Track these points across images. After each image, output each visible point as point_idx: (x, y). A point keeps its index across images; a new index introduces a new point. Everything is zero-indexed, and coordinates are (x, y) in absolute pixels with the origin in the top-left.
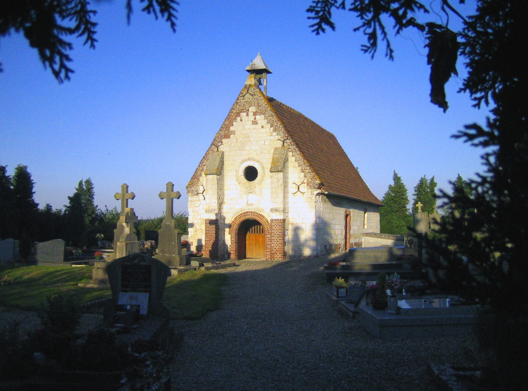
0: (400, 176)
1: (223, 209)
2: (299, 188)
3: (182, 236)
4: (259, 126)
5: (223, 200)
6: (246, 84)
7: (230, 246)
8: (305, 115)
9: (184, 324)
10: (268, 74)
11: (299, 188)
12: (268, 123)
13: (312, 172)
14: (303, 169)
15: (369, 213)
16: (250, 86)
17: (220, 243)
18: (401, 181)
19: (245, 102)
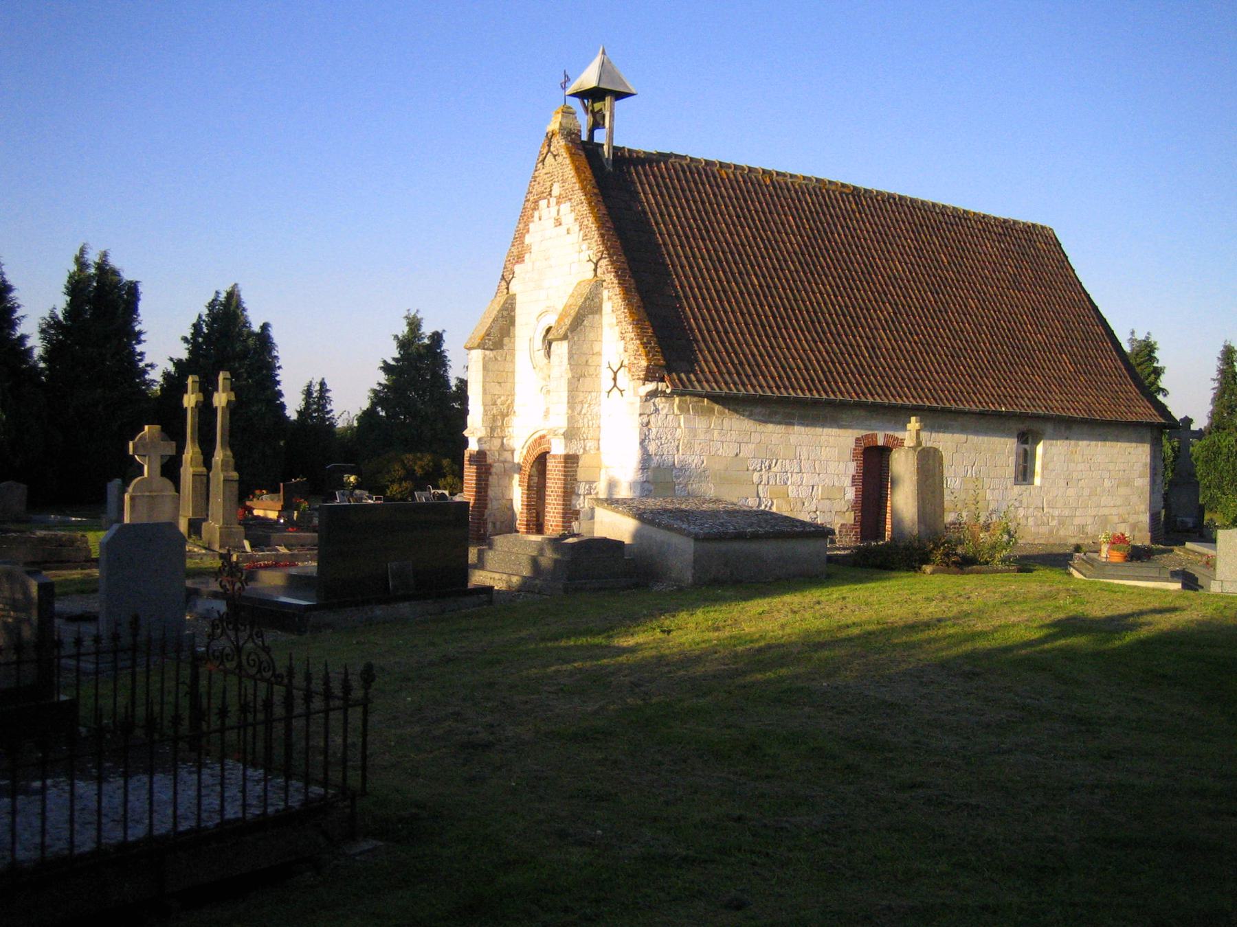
0: (395, 344)
1: (510, 429)
2: (615, 379)
3: (110, 481)
4: (563, 229)
5: (508, 407)
6: (547, 131)
7: (521, 513)
8: (936, 201)
9: (805, 700)
10: (617, 103)
11: (615, 379)
12: (576, 220)
13: (636, 339)
14: (623, 332)
15: (1048, 442)
16: (553, 135)
17: (493, 506)
18: (188, 349)
19: (546, 174)
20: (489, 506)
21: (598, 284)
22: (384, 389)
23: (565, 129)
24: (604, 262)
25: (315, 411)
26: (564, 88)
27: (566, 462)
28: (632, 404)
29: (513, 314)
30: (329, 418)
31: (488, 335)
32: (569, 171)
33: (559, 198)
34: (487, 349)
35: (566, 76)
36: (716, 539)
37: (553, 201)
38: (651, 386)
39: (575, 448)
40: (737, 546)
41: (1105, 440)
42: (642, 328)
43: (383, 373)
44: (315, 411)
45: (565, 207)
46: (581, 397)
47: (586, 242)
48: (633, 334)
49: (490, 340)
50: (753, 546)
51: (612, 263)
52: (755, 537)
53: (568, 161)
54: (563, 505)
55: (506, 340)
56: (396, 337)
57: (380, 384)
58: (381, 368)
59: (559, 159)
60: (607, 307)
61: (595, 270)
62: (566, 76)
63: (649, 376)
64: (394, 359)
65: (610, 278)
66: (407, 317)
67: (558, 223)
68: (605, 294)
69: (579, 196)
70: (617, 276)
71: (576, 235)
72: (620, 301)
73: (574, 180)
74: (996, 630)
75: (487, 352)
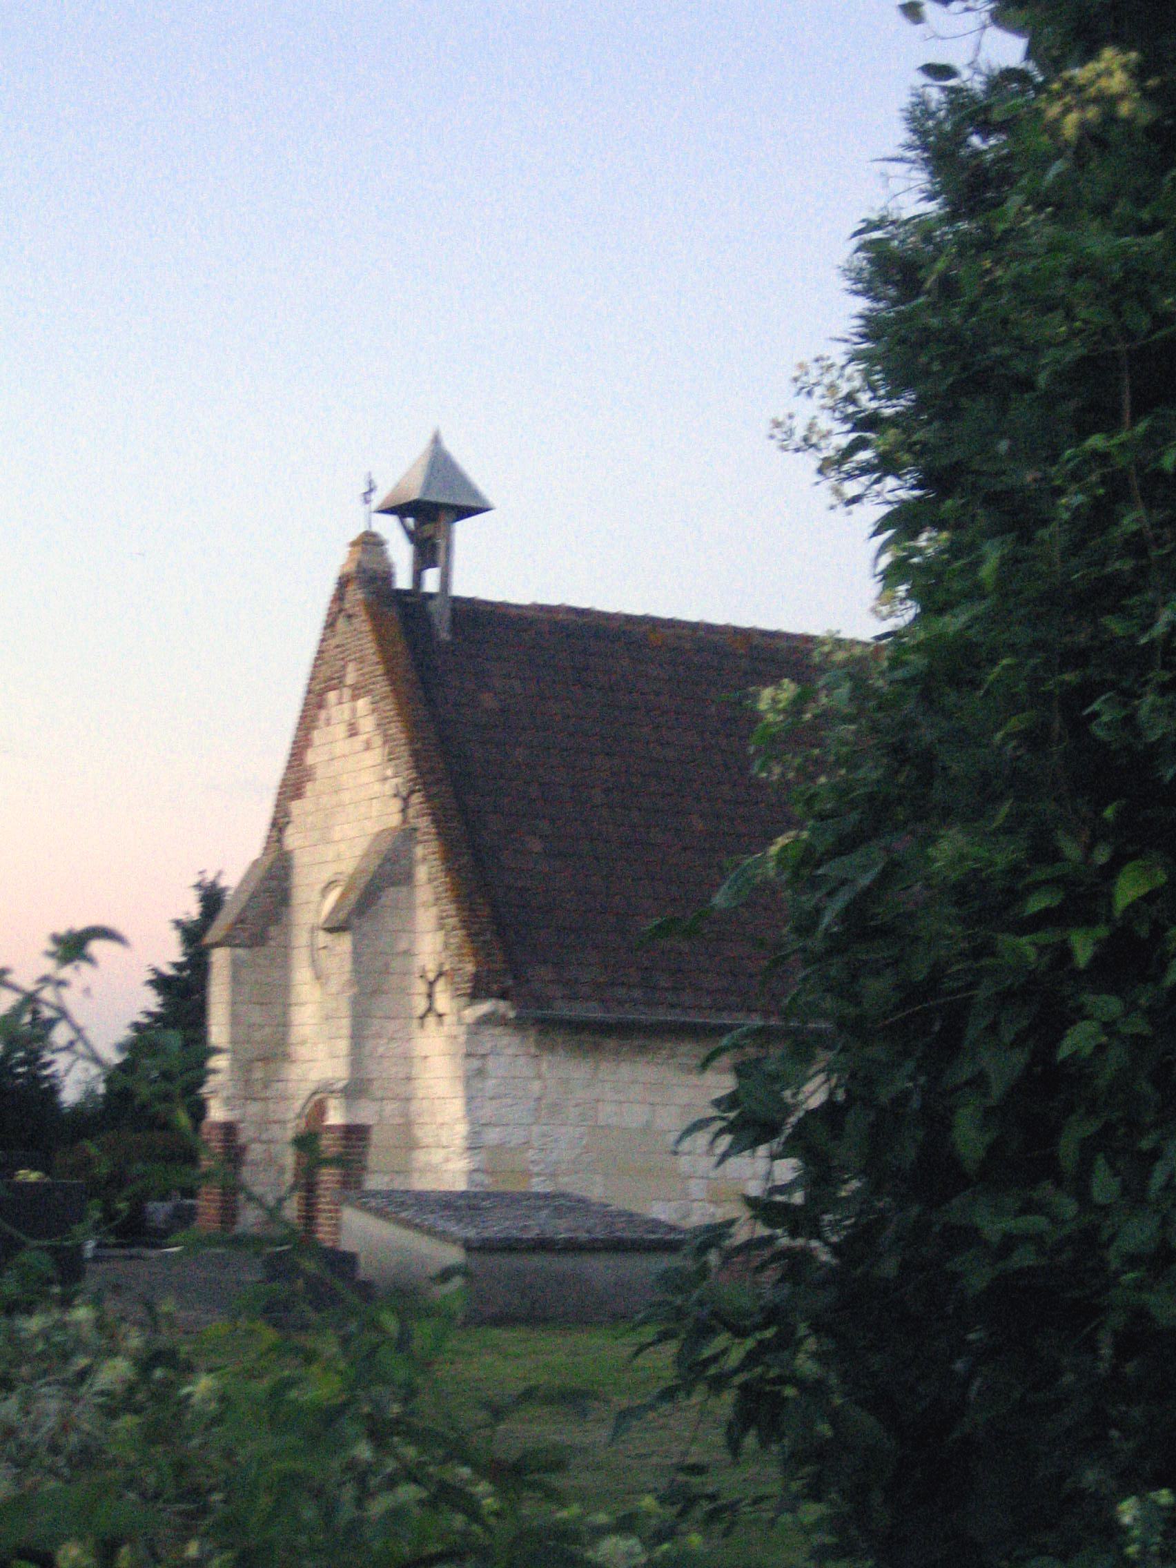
20: (241, 1219)
21: (407, 835)
22: (156, 1021)
23: (364, 571)
24: (416, 799)
25: (22, 1063)
26: (367, 501)
27: (346, 1138)
28: (455, 1037)
29: (1152, 927)
30: (47, 1077)
31: (242, 921)
32: (369, 647)
33: (354, 687)
34: (237, 946)
35: (370, 482)
36: (499, 1250)
37: (347, 693)
38: (484, 1007)
39: (365, 1114)
40: (538, 1261)
41: (208, 1015)
42: (471, 910)
43: (154, 992)
44: (22, 1063)
45: (363, 704)
46: (376, 1025)
47: (393, 763)
48: (456, 919)
49: (243, 930)
50: (565, 1264)
51: (428, 798)
52: (573, 1247)
53: (367, 627)
54: (222, 1201)
55: (273, 930)
56: (178, 924)
57: (149, 1014)
58: (151, 982)
59: (356, 621)
60: (422, 873)
61: (404, 811)
62: (370, 482)
63: (476, 993)
64: (176, 965)
65: (424, 823)
66: (198, 886)
67: (353, 731)
68: (419, 851)
69: (382, 687)
70: (436, 821)
71: (376, 755)
72: (438, 863)
73: (375, 659)
74: (623, 1335)
75: (240, 951)
